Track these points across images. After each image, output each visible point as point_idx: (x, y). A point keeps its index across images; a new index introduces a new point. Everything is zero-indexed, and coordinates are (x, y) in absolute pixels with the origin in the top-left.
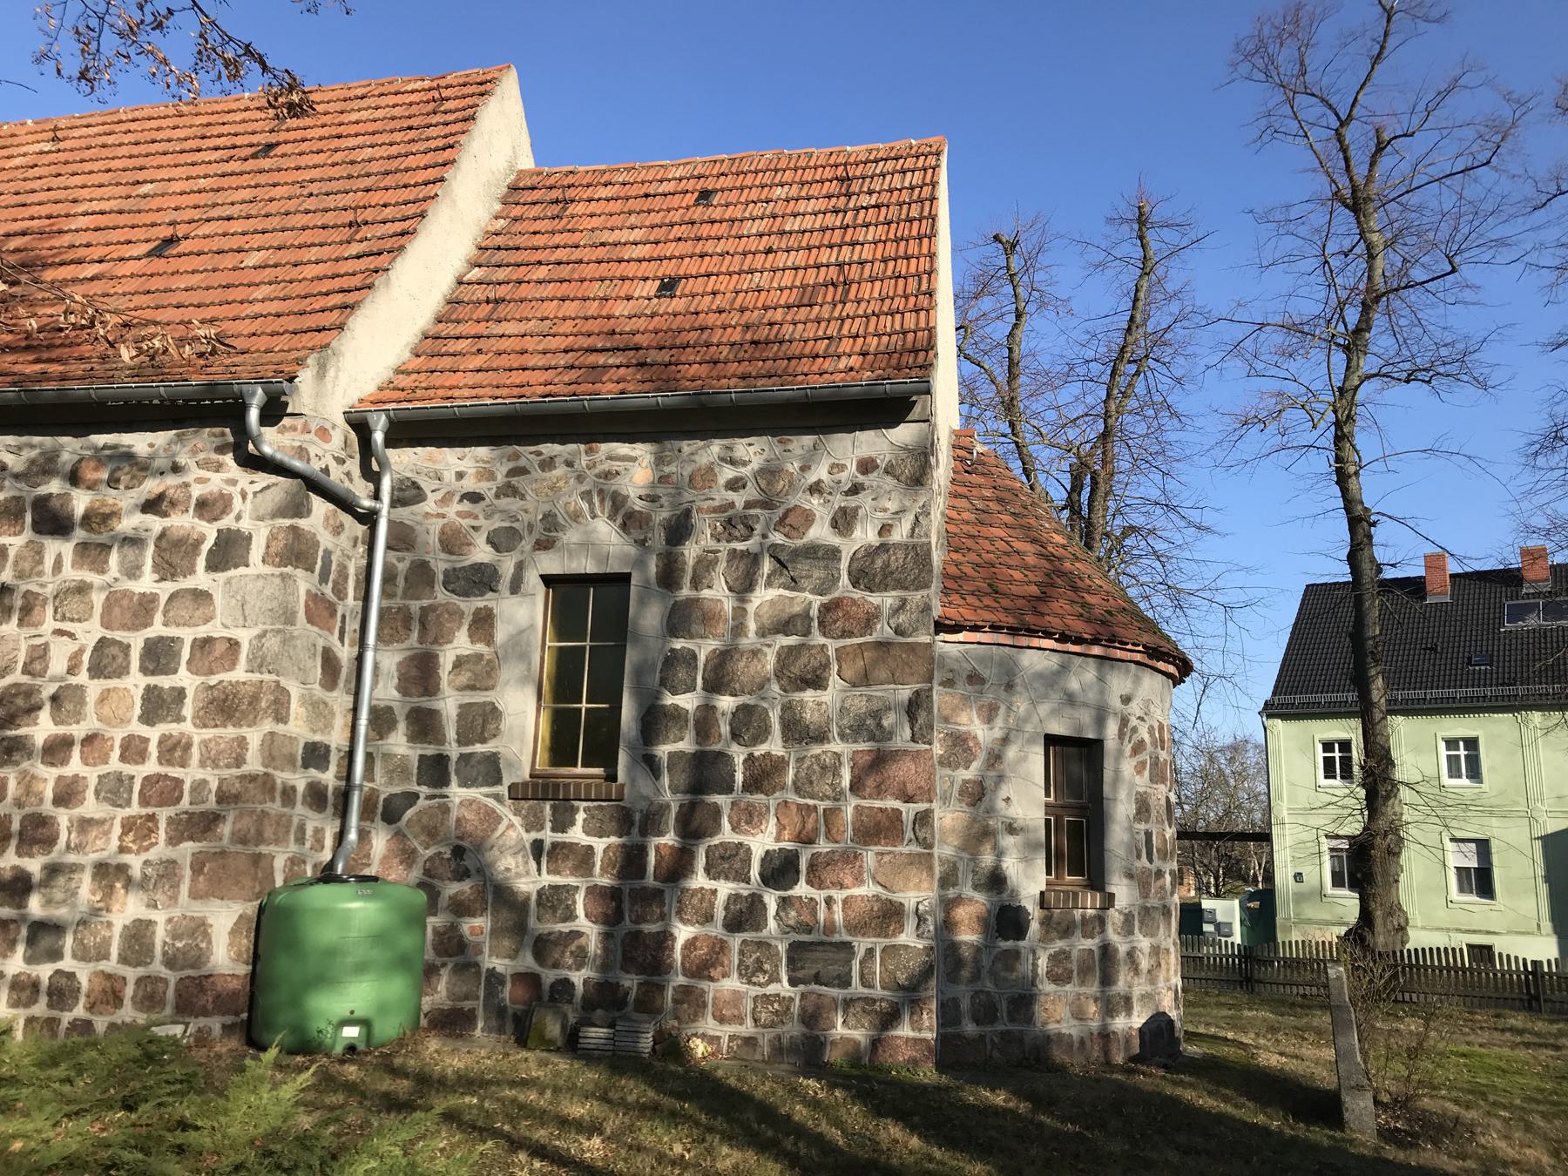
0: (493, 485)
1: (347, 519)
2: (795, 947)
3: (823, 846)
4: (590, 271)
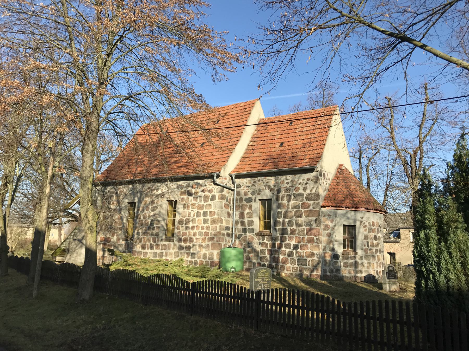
0: (251, 184)
1: (230, 191)
2: (298, 259)
3: (302, 243)
4: (269, 142)
